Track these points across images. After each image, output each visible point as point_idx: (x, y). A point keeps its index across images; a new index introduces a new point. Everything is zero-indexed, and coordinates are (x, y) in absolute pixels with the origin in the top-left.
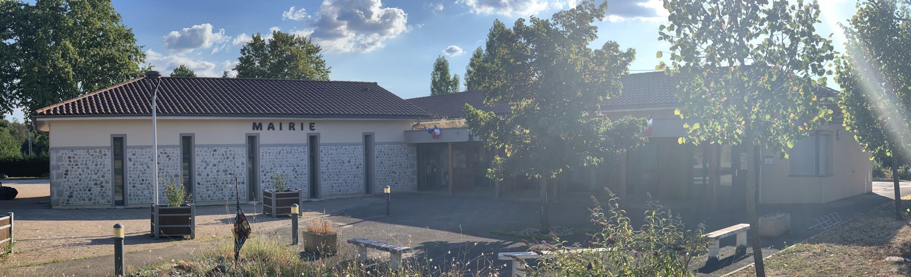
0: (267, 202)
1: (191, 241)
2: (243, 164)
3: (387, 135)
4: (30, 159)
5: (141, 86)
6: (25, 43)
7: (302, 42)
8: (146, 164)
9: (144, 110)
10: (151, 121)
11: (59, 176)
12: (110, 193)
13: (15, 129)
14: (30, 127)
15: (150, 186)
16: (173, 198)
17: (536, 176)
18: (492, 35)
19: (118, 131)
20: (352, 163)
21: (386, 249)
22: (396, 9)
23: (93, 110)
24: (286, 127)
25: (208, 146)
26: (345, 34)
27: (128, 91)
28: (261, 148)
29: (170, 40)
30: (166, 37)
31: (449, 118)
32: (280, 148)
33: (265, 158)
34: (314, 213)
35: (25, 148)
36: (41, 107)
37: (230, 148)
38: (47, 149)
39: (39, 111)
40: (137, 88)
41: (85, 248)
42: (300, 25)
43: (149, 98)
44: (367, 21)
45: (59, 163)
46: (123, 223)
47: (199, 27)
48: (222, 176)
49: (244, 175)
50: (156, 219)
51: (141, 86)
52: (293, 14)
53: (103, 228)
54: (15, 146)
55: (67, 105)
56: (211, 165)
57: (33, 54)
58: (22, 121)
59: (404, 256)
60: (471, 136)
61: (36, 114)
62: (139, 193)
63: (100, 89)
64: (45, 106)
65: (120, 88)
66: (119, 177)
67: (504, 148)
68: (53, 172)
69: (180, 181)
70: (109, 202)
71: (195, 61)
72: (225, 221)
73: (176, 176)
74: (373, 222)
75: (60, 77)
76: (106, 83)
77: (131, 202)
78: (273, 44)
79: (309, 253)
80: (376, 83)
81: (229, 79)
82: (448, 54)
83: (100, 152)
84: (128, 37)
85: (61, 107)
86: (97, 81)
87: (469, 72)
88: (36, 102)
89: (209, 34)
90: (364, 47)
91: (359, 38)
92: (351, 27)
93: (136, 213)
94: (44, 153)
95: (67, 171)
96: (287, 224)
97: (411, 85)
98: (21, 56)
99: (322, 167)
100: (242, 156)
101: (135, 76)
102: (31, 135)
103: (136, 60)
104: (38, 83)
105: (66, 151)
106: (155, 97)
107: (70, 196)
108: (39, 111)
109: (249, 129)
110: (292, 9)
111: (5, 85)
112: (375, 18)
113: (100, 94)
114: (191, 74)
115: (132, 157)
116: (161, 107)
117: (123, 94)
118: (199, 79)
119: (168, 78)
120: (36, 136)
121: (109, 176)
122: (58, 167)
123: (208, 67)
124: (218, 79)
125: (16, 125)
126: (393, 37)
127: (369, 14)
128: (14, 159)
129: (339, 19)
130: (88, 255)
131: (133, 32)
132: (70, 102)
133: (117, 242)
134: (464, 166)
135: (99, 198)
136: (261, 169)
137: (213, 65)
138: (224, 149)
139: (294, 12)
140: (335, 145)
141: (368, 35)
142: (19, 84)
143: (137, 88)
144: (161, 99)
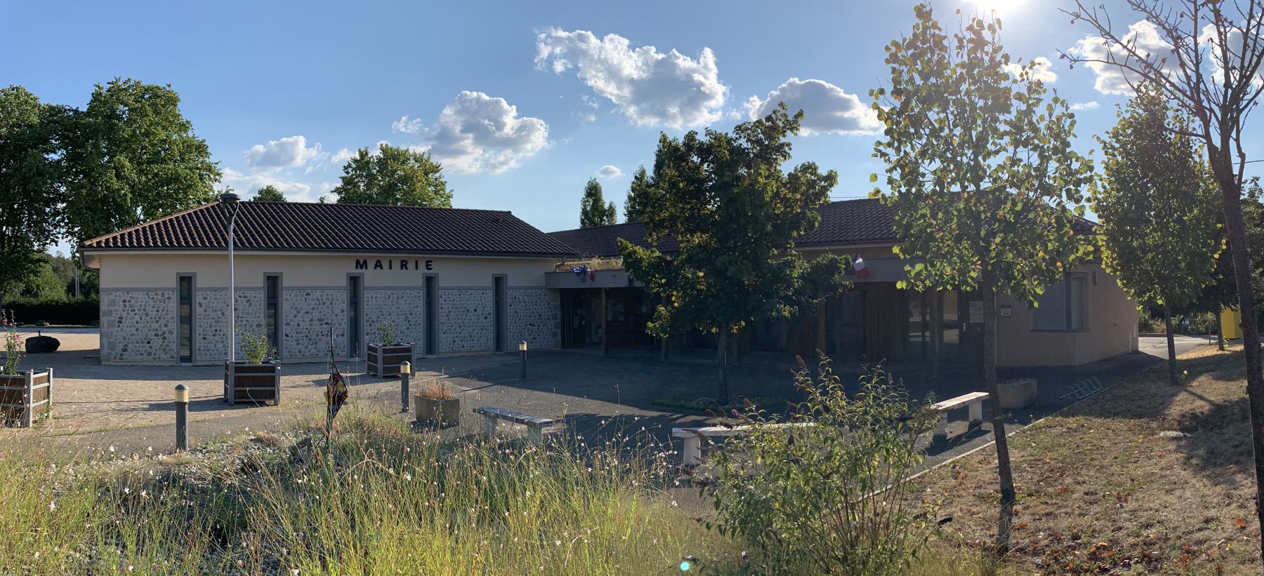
0: (372, 358)
1: (274, 408)
4: (76, 302)
9: (219, 243)
11: (111, 324)
16: (253, 354)
21: (522, 422)
22: (535, 120)
25: (300, 289)
26: (470, 149)
29: (252, 156)
35: (70, 289)
36: (90, 238)
39: (88, 243)
41: (141, 414)
44: (498, 134)
45: (112, 308)
46: (188, 385)
48: (317, 327)
53: (162, 390)
55: (122, 235)
56: (303, 312)
66: (186, 326)
71: (284, 182)
72: (319, 383)
73: (259, 325)
77: (200, 358)
78: (382, 163)
81: (326, 205)
84: (201, 149)
86: (160, 206)
90: (494, 167)
91: (487, 155)
94: (93, 295)
96: (396, 386)
97: (556, 214)
99: (441, 316)
101: (207, 200)
102: (79, 272)
107: (125, 350)
108: (88, 243)
109: (352, 270)
110: (404, 118)
111: (48, 210)
114: (280, 197)
115: (203, 301)
116: (240, 240)
117: (193, 222)
118: (289, 204)
119: (249, 203)
121: (174, 325)
122: (110, 313)
123: (301, 190)
125: (60, 260)
127: (500, 126)
130: (143, 423)
132: (126, 231)
133: (180, 407)
137: (308, 188)
138: (319, 293)
140: (458, 289)
142: (64, 209)
144: (240, 229)
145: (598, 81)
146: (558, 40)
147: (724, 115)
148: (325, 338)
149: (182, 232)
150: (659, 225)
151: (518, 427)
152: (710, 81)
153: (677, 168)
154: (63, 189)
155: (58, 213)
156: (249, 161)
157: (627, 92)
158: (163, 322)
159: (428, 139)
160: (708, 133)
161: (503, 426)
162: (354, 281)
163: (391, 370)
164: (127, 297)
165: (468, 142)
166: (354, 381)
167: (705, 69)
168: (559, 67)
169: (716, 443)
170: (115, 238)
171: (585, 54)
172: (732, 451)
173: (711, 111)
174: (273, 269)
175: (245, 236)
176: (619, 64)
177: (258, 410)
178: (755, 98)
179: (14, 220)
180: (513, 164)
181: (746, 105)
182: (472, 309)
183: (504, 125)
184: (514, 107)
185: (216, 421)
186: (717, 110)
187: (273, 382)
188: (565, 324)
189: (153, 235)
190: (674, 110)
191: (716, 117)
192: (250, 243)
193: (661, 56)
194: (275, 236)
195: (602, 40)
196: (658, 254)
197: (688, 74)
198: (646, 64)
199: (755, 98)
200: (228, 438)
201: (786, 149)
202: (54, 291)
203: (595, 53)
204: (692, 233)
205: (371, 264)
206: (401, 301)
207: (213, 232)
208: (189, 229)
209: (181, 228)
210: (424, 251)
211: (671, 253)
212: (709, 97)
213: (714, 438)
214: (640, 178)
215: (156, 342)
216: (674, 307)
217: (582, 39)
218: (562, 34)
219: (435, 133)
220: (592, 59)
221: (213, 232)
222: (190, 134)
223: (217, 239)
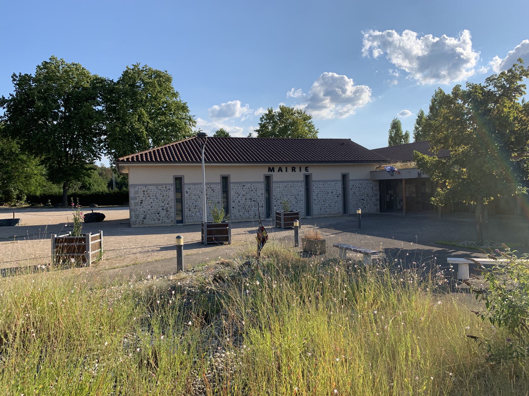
0: (278, 219)
1: (228, 246)
2: (262, 194)
3: (357, 174)
4: (114, 193)
5: (194, 143)
6: (109, 109)
8: (198, 195)
9: (196, 159)
10: (201, 166)
11: (136, 204)
12: (173, 215)
13: (103, 171)
14: (114, 170)
15: (201, 210)
16: (217, 218)
17: (472, 203)
18: (434, 101)
19: (179, 173)
20: (334, 193)
21: (360, 252)
22: (363, 86)
23: (161, 159)
24: (290, 169)
25: (239, 183)
26: (328, 106)
27: (184, 146)
28: (274, 184)
29: (213, 112)
30: (210, 110)
31: (403, 162)
34: (309, 226)
35: (110, 185)
36: (122, 156)
37: (253, 184)
38: (127, 185)
39: (121, 159)
40: (191, 144)
41: (156, 253)
42: (299, 101)
43: (200, 152)
44: (343, 96)
45: (136, 195)
46: (182, 235)
47: (232, 103)
48: (248, 202)
49: (263, 202)
50: (205, 232)
51: (194, 143)
52: (294, 93)
53: (169, 239)
54: (103, 184)
55: (141, 155)
56: (241, 195)
57: (116, 118)
58: (107, 165)
59: (373, 257)
60: (419, 174)
61: (119, 161)
62: (193, 214)
63: (165, 144)
64: (126, 155)
65: (179, 144)
66: (180, 204)
67: (445, 182)
68: (132, 202)
69: (221, 206)
70: (172, 221)
72: (251, 232)
73: (218, 203)
75: (136, 135)
76: (170, 141)
77: (187, 221)
78: (281, 115)
79: (307, 252)
80: (350, 139)
81: (252, 139)
82: (401, 116)
83: (166, 187)
84: (184, 108)
85: (137, 156)
86: (163, 139)
87: (416, 128)
88: (119, 153)
90: (341, 114)
91: (338, 108)
93: (191, 228)
94: (125, 189)
96: (291, 233)
97: (375, 140)
98: (107, 119)
100: (261, 188)
101: (190, 136)
102: (115, 176)
103: (190, 125)
104: (120, 139)
105: (141, 187)
106: (204, 150)
107: (145, 218)
108: (121, 159)
110: (293, 89)
111: (95, 139)
112: (349, 93)
114: (228, 134)
115: (188, 190)
116: (207, 157)
117: (181, 148)
118: (232, 138)
119: (212, 138)
120: (119, 177)
121: (172, 204)
122: (135, 198)
123: (238, 130)
124: (245, 139)
125: (103, 169)
126: (361, 106)
127: (344, 91)
128: (102, 193)
129: (325, 95)
130: (158, 258)
131: (187, 105)
132: (144, 153)
133: (179, 248)
134: (414, 195)
135: (165, 219)
136: (274, 198)
137: (242, 129)
138: (249, 185)
139: (294, 92)
140: (323, 181)
142: (105, 139)
143: (191, 144)
144: (207, 151)
145: (397, 60)
146: (375, 38)
147: (476, 71)
149: (176, 153)
150: (438, 142)
151: (359, 255)
152: (468, 51)
153: (449, 108)
154: (104, 128)
155: (102, 142)
156: (211, 114)
157: (415, 65)
160: (468, 85)
161: (350, 254)
162: (268, 178)
163: (288, 224)
165: (327, 101)
166: (271, 230)
167: (464, 44)
168: (376, 53)
169: (486, 268)
171: (390, 44)
172: (497, 273)
173: (467, 70)
174: (225, 173)
175: (210, 155)
176: (411, 48)
177: (220, 247)
178: (497, 57)
179: (74, 144)
180: (351, 112)
181: (491, 63)
184: (352, 80)
186: (471, 69)
187: (227, 232)
188: (381, 200)
190: (444, 73)
191: (471, 73)
192: (213, 159)
193: (437, 39)
194: (226, 155)
195: (401, 35)
196: (437, 159)
197: (453, 49)
198: (427, 46)
199: (497, 57)
200: (205, 263)
201: (522, 89)
202: (100, 186)
203: (397, 43)
204: (459, 145)
205: (276, 170)
206: (292, 188)
207: (193, 153)
208: (179, 151)
209: (175, 151)
211: (444, 158)
212: (466, 61)
213: (485, 265)
214: (421, 117)
215: (163, 213)
216: (448, 189)
217: (390, 35)
218: (377, 33)
220: (395, 47)
221: (193, 153)
223: (195, 157)
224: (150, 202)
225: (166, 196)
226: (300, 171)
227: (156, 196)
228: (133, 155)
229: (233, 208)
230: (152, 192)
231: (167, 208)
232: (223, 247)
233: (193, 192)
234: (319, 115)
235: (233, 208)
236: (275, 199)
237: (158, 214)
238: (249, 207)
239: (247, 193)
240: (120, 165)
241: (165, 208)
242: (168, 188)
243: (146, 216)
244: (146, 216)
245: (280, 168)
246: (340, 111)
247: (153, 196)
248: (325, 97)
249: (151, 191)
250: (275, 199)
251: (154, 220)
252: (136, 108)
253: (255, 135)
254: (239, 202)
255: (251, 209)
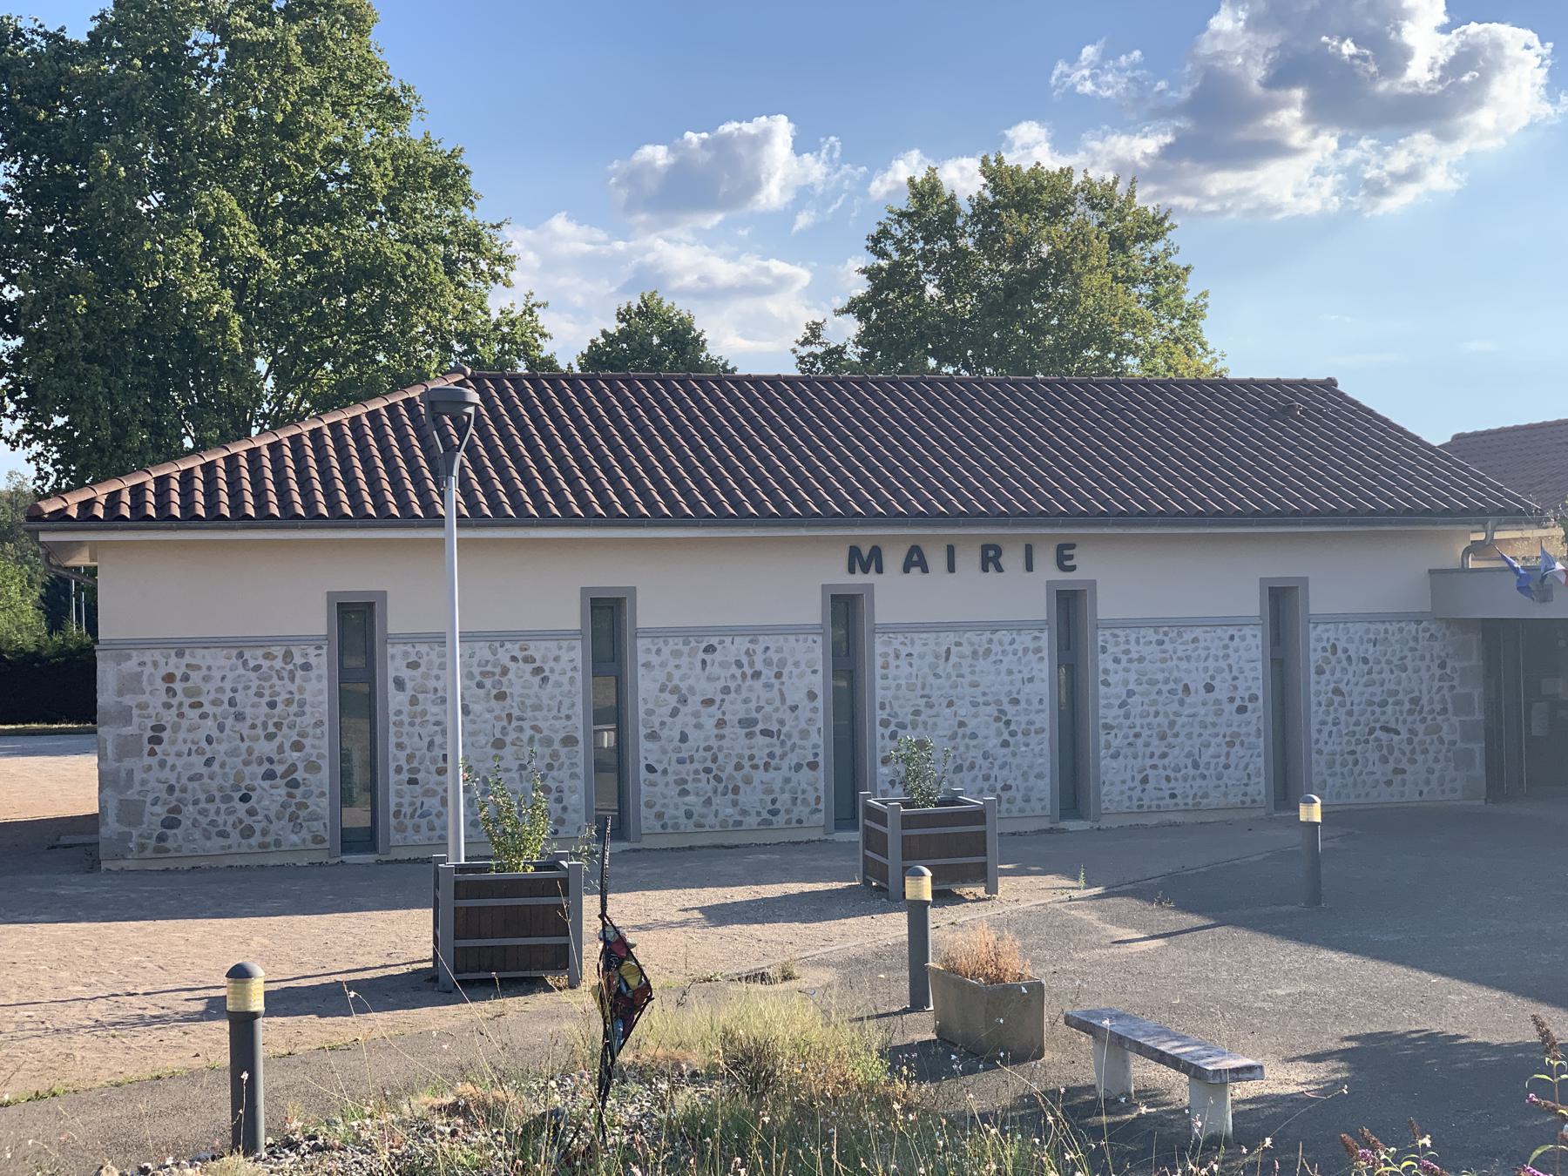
1: (566, 996)
2: (812, 696)
3: (1358, 587)
7: (1099, 198)
10: (441, 543)
19: (356, 579)
20: (1222, 693)
22: (1503, 31)
24: (969, 559)
25: (686, 634)
26: (1298, 137)
29: (633, 178)
32: (949, 639)
33: (893, 676)
37: (764, 641)
41: (173, 1034)
44: (1382, 87)
45: (128, 700)
47: (749, 128)
49: (816, 738)
56: (694, 702)
63: (201, 446)
65: (373, 416)
70: (318, 840)
71: (732, 258)
74: (1244, 934)
80: (1330, 384)
83: (288, 656)
84: (446, 178)
86: (327, 354)
89: (781, 158)
90: (1377, 190)
91: (1351, 155)
92: (1321, 112)
95: (159, 728)
96: (893, 927)
99: (1106, 703)
107: (171, 823)
109: (838, 575)
110: (1088, 52)
113: (391, 409)
115: (405, 673)
121: (320, 745)
122: (125, 716)
123: (782, 282)
126: (1490, 144)
127: (1393, 57)
130: (173, 1062)
135: (281, 828)
136: (881, 715)
138: (742, 644)
140: (1155, 624)
141: (1392, 140)
148: (760, 775)
149: (347, 470)
156: (623, 193)
158: (287, 736)
159: (1161, 113)
161: (1144, 1072)
162: (846, 610)
164: (176, 666)
170: (137, 491)
174: (608, 576)
180: (1438, 179)
182: (1197, 681)
183: (1406, 53)
185: (379, 1046)
189: (258, 480)
205: (893, 559)
206: (981, 664)
208: (367, 460)
210: (1049, 517)
219: (1185, 94)
222: (415, 129)
224: (201, 735)
225: (289, 702)
226: (1029, 568)
227: (232, 703)
228: (114, 486)
229: (651, 769)
230: (212, 686)
231: (293, 768)
232: (540, 1000)
233: (432, 683)
234: (1241, 193)
235: (651, 769)
236: (885, 724)
237: (245, 798)
238: (739, 767)
239: (726, 690)
240: (43, 537)
241: (279, 769)
242: (299, 660)
243: (177, 810)
244: (177, 810)
245: (915, 550)
246: (1371, 173)
247: (215, 703)
248: (1279, 94)
249: (206, 679)
250: (885, 724)
251: (223, 834)
252: (185, 183)
253: (846, 332)
254: (684, 738)
255: (748, 781)
